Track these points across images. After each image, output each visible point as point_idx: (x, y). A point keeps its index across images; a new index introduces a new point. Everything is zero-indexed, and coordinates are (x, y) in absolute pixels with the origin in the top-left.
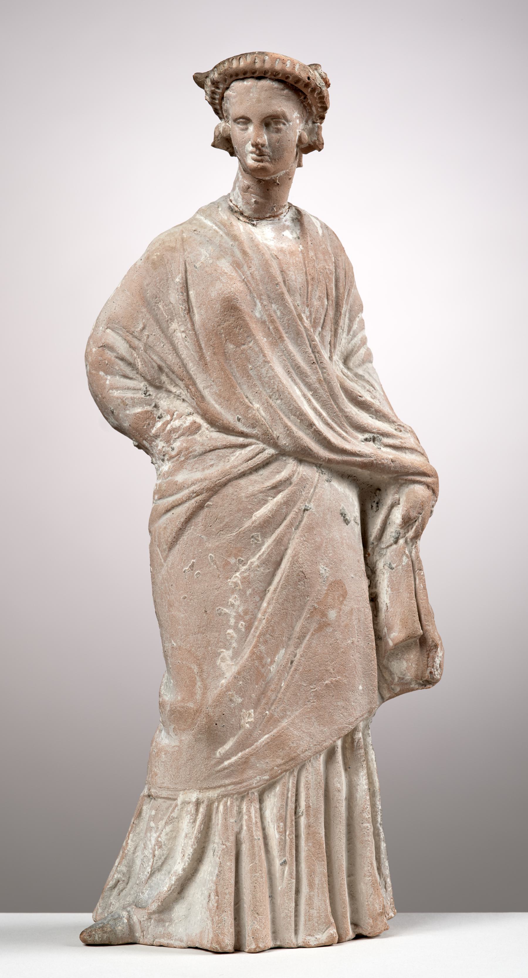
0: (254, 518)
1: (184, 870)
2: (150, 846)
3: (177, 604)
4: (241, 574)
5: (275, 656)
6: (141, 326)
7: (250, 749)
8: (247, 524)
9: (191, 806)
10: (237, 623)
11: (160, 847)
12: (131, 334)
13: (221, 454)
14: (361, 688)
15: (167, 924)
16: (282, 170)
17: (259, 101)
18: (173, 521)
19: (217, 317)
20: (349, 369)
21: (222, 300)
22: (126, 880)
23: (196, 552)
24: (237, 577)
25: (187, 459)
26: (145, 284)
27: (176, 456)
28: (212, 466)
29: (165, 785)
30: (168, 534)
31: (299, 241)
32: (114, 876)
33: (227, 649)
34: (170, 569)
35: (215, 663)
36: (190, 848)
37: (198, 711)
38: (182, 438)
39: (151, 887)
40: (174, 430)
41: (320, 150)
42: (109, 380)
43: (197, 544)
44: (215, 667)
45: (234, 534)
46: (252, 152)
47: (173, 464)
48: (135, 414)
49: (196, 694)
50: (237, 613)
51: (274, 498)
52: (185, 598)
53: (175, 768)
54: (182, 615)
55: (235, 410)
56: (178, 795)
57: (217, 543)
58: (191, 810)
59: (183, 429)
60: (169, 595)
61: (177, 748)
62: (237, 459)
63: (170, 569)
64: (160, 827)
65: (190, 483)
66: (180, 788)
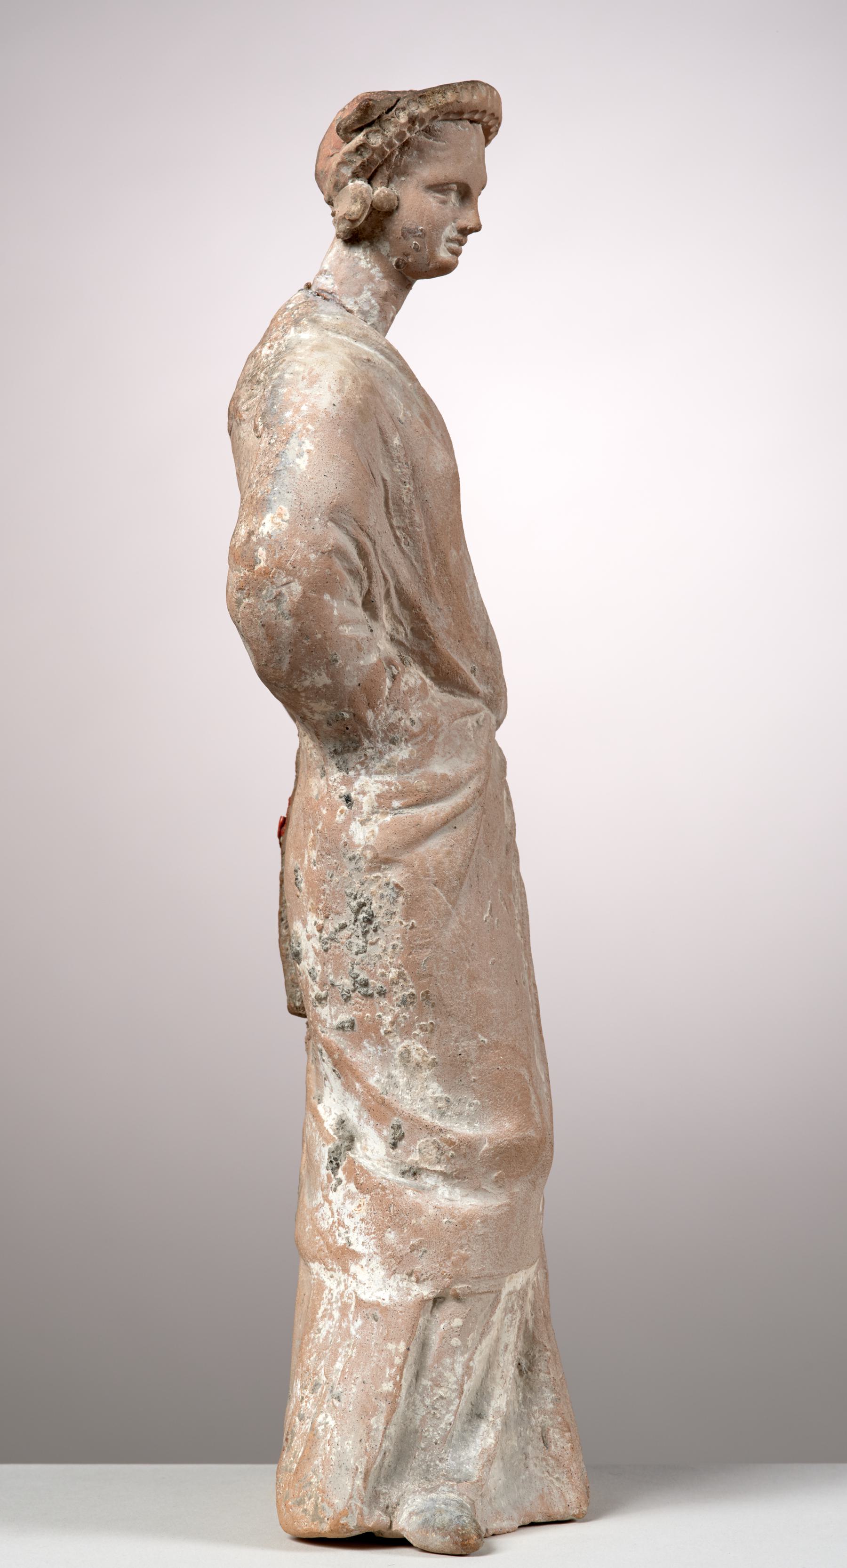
2: (453, 1379)
18: (462, 840)
29: (486, 1272)
30: (459, 862)
34: (466, 919)
47: (417, 747)
61: (506, 1209)
63: (466, 919)
64: (469, 1343)
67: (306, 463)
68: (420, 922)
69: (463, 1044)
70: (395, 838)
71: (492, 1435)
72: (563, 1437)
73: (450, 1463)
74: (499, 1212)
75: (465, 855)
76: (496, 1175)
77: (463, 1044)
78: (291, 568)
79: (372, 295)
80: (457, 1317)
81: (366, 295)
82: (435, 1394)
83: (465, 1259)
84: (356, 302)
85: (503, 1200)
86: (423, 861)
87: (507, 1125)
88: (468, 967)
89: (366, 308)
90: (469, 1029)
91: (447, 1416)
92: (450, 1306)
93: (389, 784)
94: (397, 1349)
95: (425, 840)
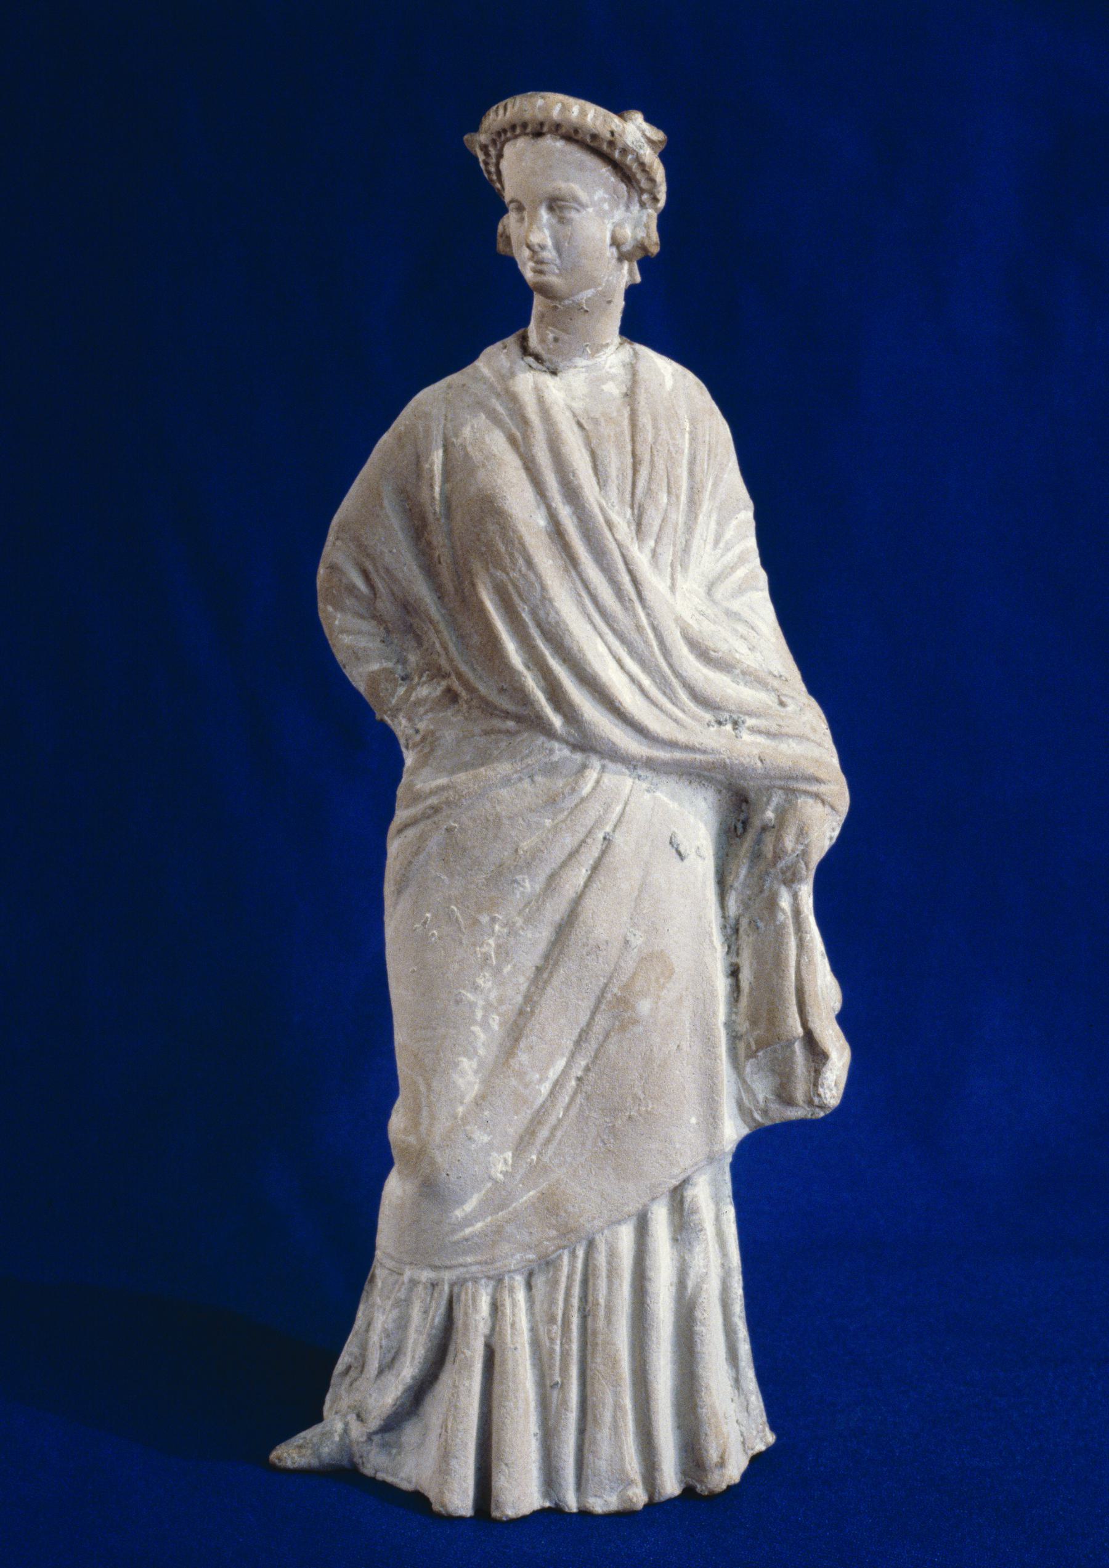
1: (414, 1378)
5: (547, 1069)
7: (504, 1212)
14: (693, 1120)
15: (394, 1451)
16: (589, 287)
20: (714, 602)
32: (344, 1360)
33: (470, 1058)
39: (379, 1389)
40: (418, 703)
50: (486, 1000)
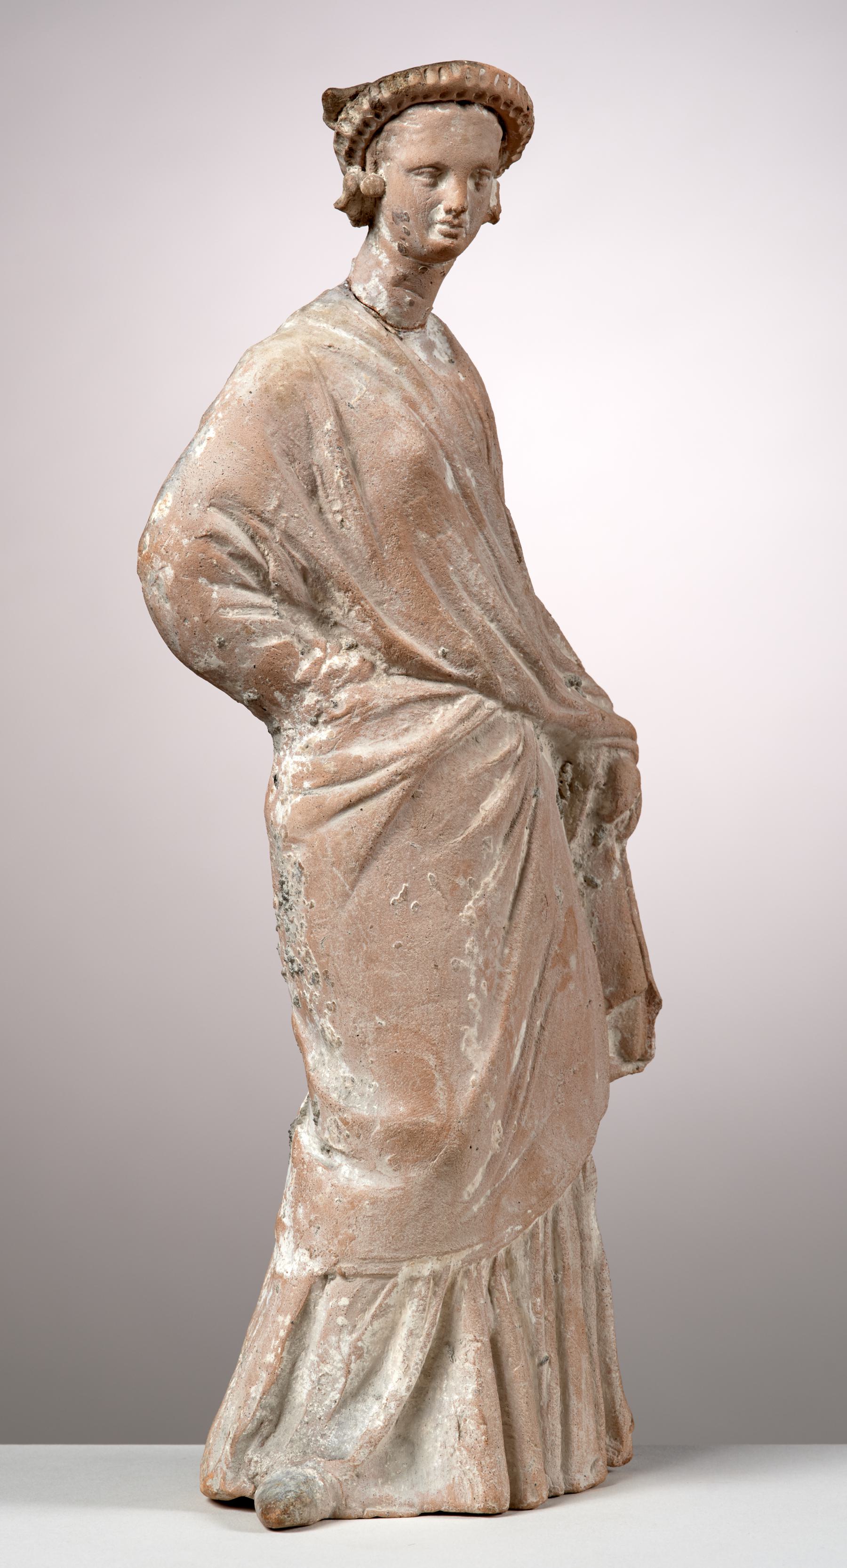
0: (482, 813)
1: (408, 1389)
3: (384, 958)
4: (474, 903)
6: (275, 503)
8: (476, 823)
9: (420, 1283)
10: (478, 981)
11: (360, 1357)
12: (258, 516)
13: (416, 712)
17: (465, 140)
18: (366, 822)
19: (403, 489)
21: (411, 460)
22: (275, 1419)
23: (408, 871)
24: (469, 910)
25: (364, 720)
26: (269, 432)
27: (343, 716)
28: (407, 730)
30: (359, 843)
31: (453, 366)
33: (472, 1026)
34: (366, 901)
35: (458, 1049)
36: (418, 1352)
37: (444, 1129)
38: (349, 686)
40: (334, 674)
41: (494, 219)
42: (217, 592)
43: (408, 857)
44: (459, 1055)
45: (460, 839)
46: (443, 223)
47: (338, 729)
48: (268, 649)
49: (436, 1101)
51: (501, 778)
52: (399, 946)
53: (395, 1225)
54: (397, 975)
55: (437, 639)
56: (400, 1269)
57: (438, 855)
58: (421, 1291)
59: (351, 671)
60: (367, 944)
61: (399, 1193)
62: (442, 719)
65: (387, 759)
66: (403, 1256)
67: (202, 451)
68: (318, 902)
69: (361, 1025)
70: (299, 818)
71: (382, 1418)
72: (478, 1428)
73: (332, 1439)
74: (391, 1195)
75: (366, 837)
76: (389, 1157)
77: (361, 1025)
78: (164, 553)
79: (380, 280)
80: (345, 1296)
81: (375, 281)
82: (320, 1371)
83: (353, 1239)
84: (364, 289)
85: (398, 1183)
86: (322, 841)
87: (402, 1109)
88: (365, 948)
89: (374, 294)
90: (366, 1010)
91: (332, 1394)
92: (337, 1282)
93: (303, 764)
94: (283, 1322)
95: (328, 820)
